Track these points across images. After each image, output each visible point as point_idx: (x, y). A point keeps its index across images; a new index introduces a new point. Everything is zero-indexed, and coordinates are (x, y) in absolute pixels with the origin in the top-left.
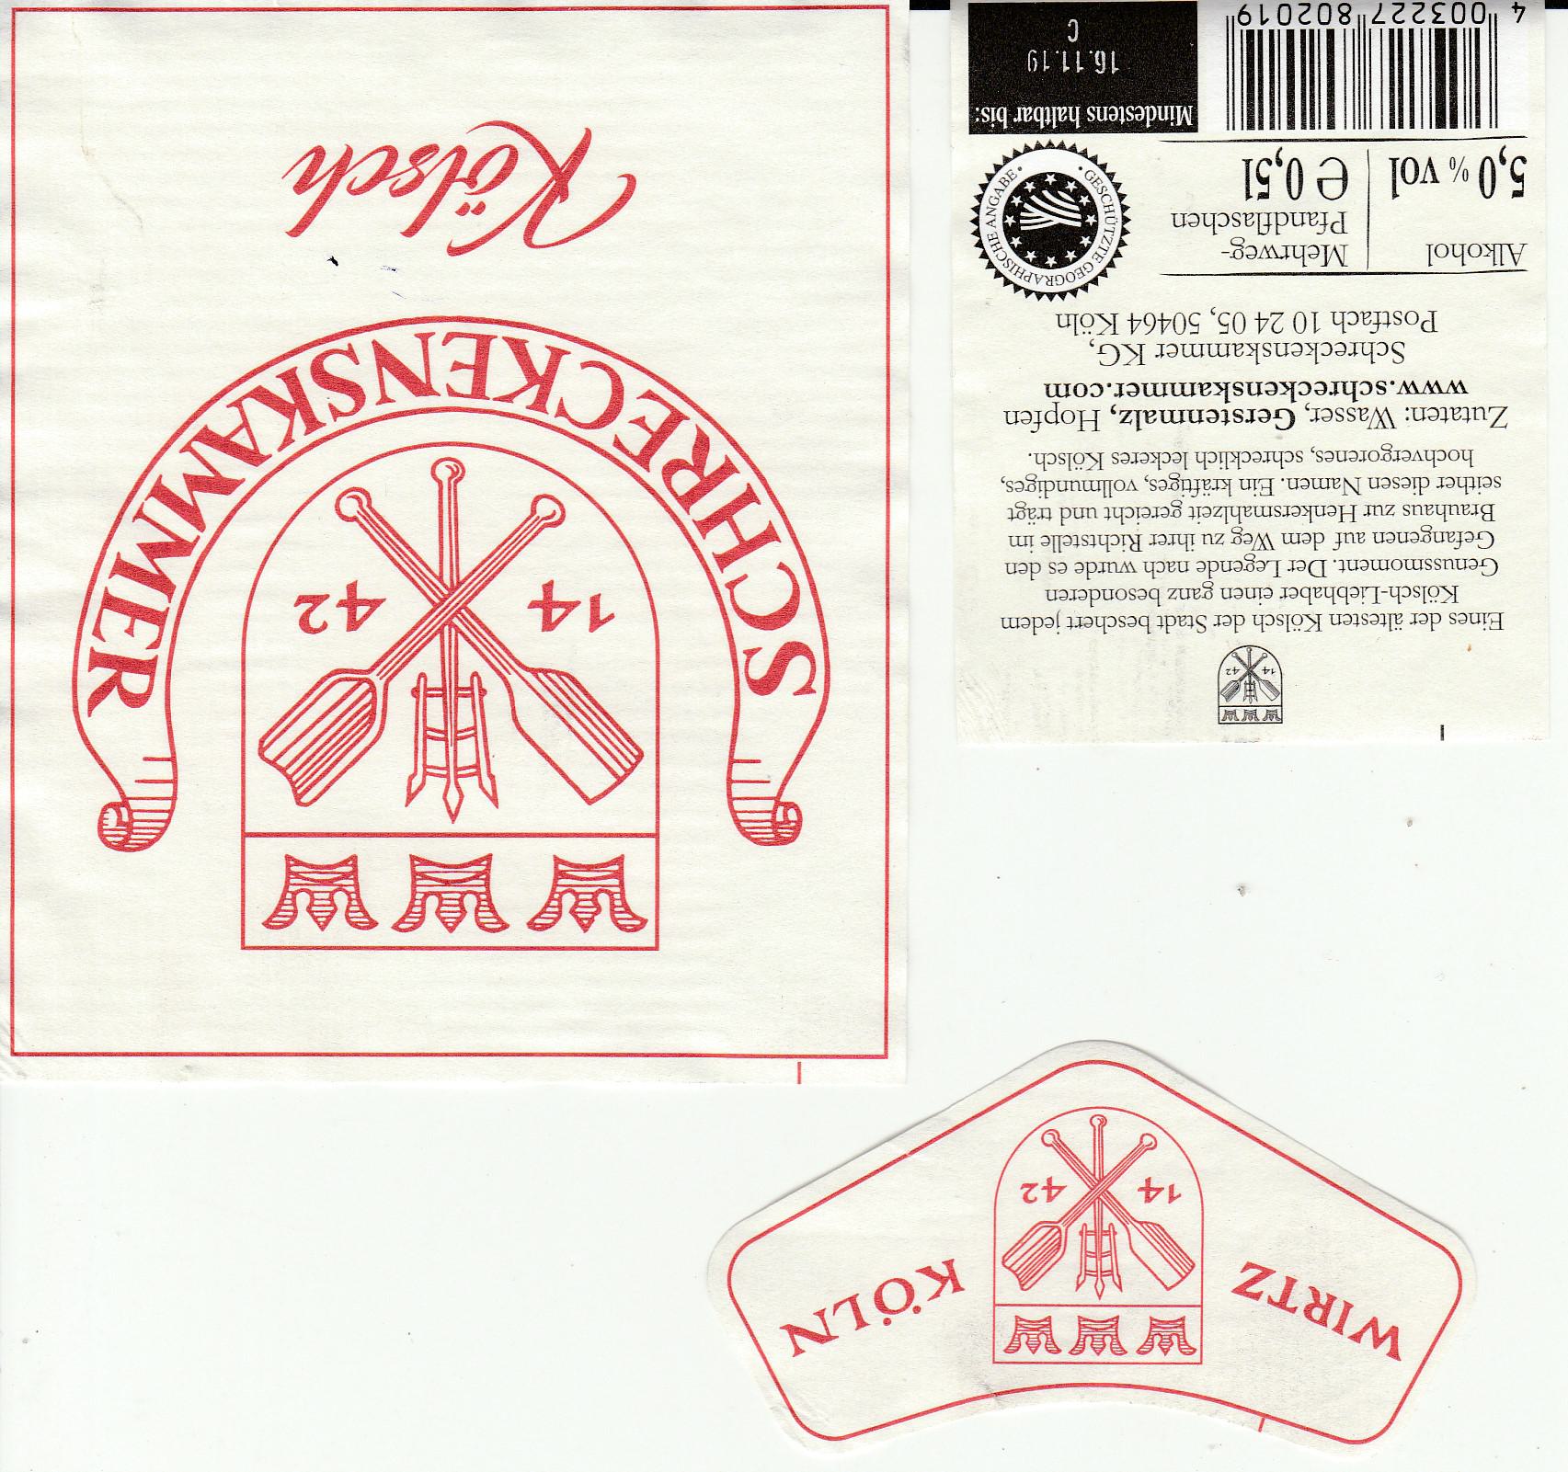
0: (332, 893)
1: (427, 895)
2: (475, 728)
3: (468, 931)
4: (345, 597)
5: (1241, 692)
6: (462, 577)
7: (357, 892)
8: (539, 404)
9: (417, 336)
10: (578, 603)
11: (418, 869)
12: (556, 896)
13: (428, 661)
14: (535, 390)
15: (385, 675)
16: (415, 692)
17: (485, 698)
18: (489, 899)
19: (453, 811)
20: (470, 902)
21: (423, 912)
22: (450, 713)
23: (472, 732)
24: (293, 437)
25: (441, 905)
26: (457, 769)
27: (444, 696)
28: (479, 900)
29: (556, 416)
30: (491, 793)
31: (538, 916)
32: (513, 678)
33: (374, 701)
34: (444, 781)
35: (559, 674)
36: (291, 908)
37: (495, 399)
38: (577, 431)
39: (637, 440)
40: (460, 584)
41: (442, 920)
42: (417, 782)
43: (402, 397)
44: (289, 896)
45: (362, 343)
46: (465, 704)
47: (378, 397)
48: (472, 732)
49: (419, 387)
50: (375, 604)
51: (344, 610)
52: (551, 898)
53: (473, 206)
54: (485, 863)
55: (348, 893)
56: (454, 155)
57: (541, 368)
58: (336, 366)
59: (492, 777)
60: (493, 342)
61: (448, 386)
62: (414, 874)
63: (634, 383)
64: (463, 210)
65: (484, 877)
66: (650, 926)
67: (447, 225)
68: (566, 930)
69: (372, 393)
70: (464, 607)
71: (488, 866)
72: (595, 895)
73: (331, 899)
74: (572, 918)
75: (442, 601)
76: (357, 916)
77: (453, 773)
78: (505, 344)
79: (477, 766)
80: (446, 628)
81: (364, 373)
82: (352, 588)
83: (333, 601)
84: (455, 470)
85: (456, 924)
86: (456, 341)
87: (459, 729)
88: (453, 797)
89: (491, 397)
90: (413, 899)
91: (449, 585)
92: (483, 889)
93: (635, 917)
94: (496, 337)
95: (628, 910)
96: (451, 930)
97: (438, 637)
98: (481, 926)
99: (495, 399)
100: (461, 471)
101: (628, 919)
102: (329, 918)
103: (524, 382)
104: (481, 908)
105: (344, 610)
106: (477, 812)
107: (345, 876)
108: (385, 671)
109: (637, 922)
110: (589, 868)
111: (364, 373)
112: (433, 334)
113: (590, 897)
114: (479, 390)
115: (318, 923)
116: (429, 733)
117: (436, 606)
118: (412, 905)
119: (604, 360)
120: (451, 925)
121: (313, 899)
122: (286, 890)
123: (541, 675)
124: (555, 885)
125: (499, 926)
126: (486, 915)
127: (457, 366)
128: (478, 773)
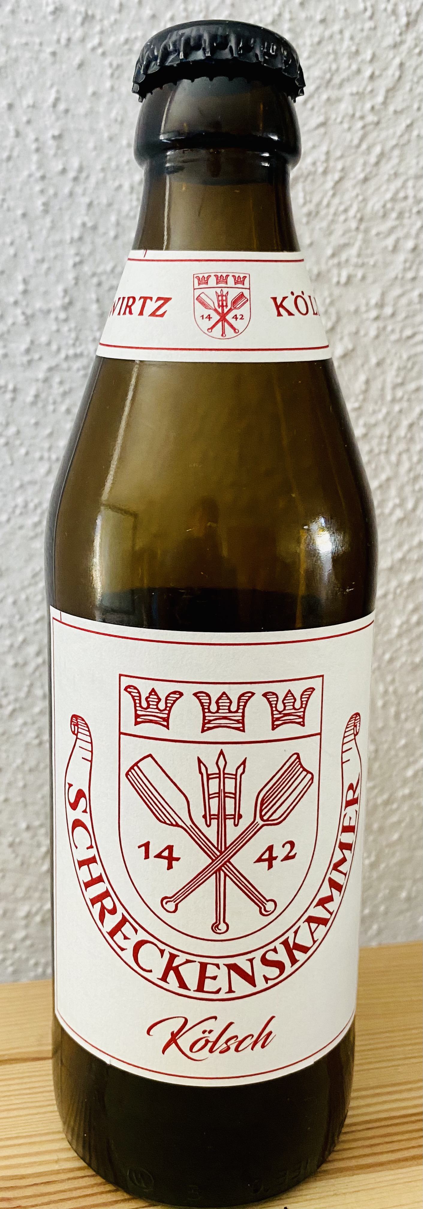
0: (284, 709)
1: (236, 712)
2: (209, 798)
3: (215, 692)
4: (274, 862)
5: (230, 299)
6: (214, 875)
7: (272, 711)
8: (173, 957)
9: (234, 992)
10: (155, 857)
11: (241, 725)
12: (168, 709)
13: (232, 833)
14: (175, 964)
15: (255, 824)
16: (240, 816)
17: (203, 813)
18: (203, 709)
19: (222, 756)
20: (214, 708)
21: (239, 702)
22: (222, 807)
23: (211, 796)
24: (294, 934)
25: (229, 707)
26: (219, 777)
27: (225, 815)
28: (209, 709)
29: (165, 950)
30: (202, 765)
31: (177, 699)
32: (189, 823)
33: (261, 811)
34: (226, 772)
35: (165, 823)
36: (303, 700)
37: (195, 961)
38: (155, 940)
39: (127, 929)
40: (215, 872)
41: (229, 698)
42: (240, 770)
43: (243, 963)
44: (304, 706)
45: (261, 984)
46: (214, 811)
47: (254, 961)
48: (211, 796)
49: (234, 968)
50: (233, 318)
51: (274, 855)
52: (171, 708)
53: (207, 1033)
54: (205, 728)
55: (277, 710)
56: (214, 1050)
57: (172, 973)
58: (273, 972)
59: (201, 772)
60: (196, 988)
61: (219, 968)
62: (243, 723)
63: (128, 955)
64: (210, 1032)
65: (206, 721)
66: (123, 688)
67: (217, 1027)
68: (163, 690)
69: (257, 963)
70: (213, 861)
71: (203, 726)
72: (148, 707)
73: (285, 707)
74: (160, 697)
75: (225, 863)
76: (273, 699)
77: (221, 775)
78: (189, 986)
79: (208, 779)
80: (223, 849)
81: (260, 970)
82: (270, 866)
83: (279, 859)
84: (216, 929)
85: (221, 696)
86: (215, 990)
87: (217, 799)
88: (221, 763)
89: (197, 963)
90: (244, 709)
91: (221, 872)
92: (207, 714)
93: (130, 693)
94: (194, 991)
95: (133, 697)
96: (224, 693)
97: (228, 845)
98: (208, 695)
99: (195, 961)
100: (214, 928)
101: (133, 692)
102: (286, 696)
103: (180, 968)
104: (207, 704)
105: (274, 855)
106: (209, 755)
107: (278, 719)
108: (256, 826)
109: (129, 690)
110: (151, 721)
111: (260, 970)
112: (226, 993)
113: (151, 706)
114: (203, 967)
115: (292, 694)
116: (233, 796)
117: (228, 861)
118: (245, 706)
119: (143, 972)
120: (225, 696)
121: (293, 705)
122: (305, 708)
123: (174, 823)
124: (169, 714)
125: (199, 695)
126: (205, 700)
127: (214, 978)
128: (208, 775)
